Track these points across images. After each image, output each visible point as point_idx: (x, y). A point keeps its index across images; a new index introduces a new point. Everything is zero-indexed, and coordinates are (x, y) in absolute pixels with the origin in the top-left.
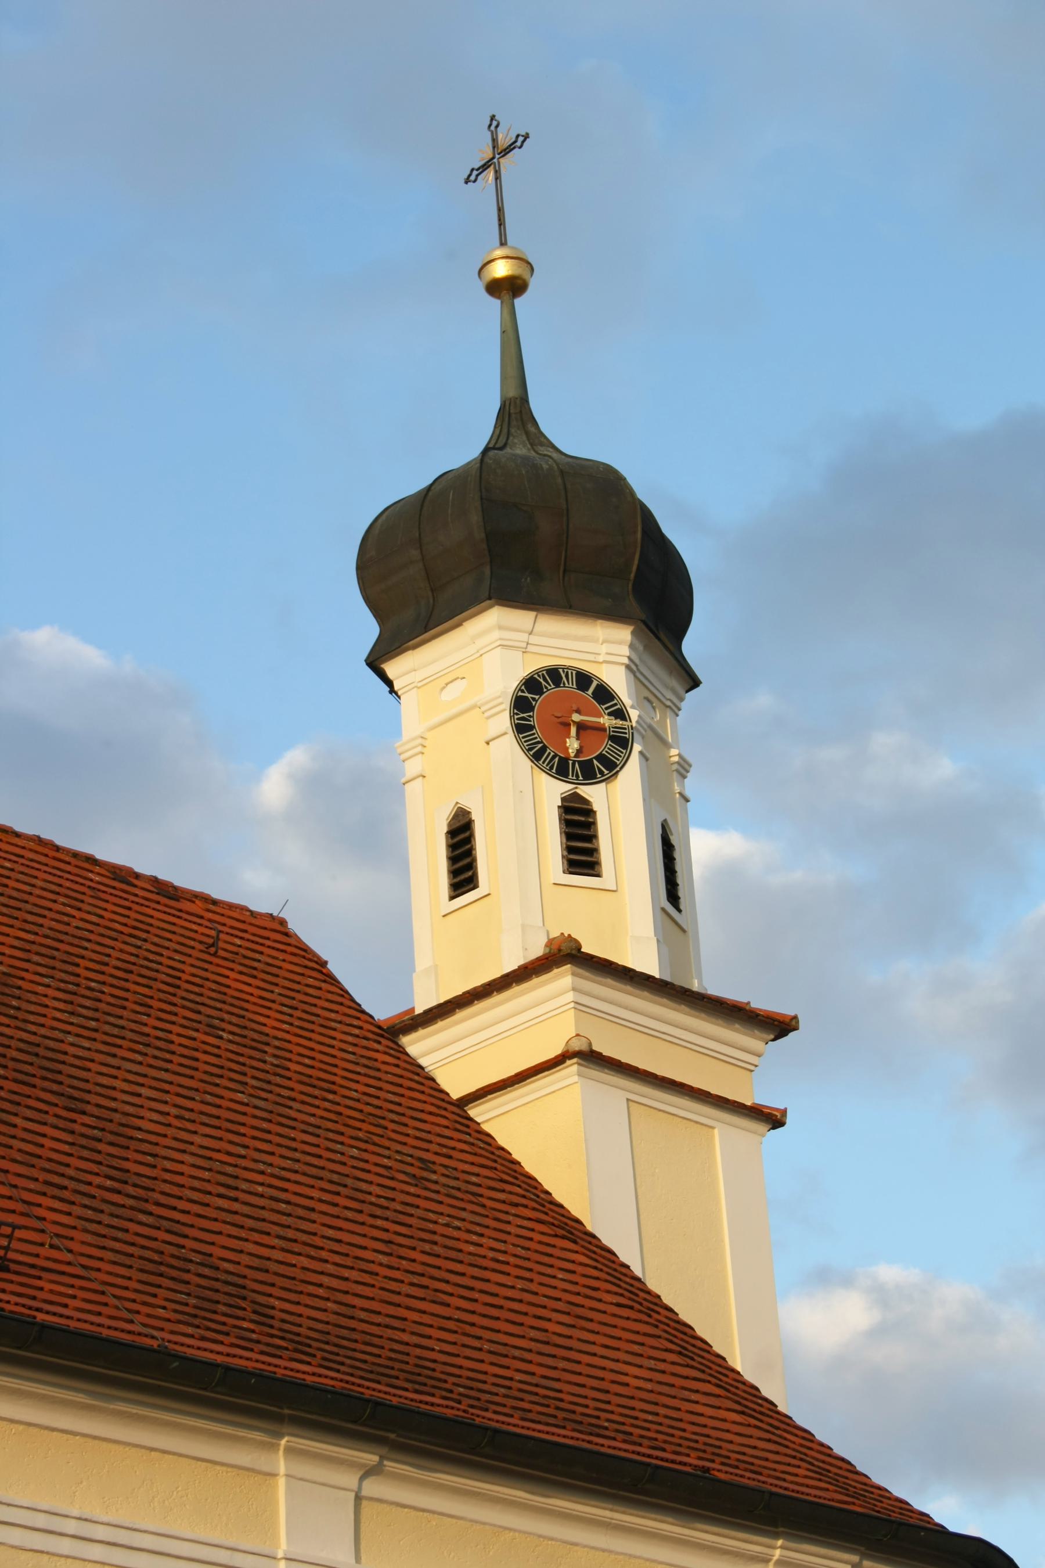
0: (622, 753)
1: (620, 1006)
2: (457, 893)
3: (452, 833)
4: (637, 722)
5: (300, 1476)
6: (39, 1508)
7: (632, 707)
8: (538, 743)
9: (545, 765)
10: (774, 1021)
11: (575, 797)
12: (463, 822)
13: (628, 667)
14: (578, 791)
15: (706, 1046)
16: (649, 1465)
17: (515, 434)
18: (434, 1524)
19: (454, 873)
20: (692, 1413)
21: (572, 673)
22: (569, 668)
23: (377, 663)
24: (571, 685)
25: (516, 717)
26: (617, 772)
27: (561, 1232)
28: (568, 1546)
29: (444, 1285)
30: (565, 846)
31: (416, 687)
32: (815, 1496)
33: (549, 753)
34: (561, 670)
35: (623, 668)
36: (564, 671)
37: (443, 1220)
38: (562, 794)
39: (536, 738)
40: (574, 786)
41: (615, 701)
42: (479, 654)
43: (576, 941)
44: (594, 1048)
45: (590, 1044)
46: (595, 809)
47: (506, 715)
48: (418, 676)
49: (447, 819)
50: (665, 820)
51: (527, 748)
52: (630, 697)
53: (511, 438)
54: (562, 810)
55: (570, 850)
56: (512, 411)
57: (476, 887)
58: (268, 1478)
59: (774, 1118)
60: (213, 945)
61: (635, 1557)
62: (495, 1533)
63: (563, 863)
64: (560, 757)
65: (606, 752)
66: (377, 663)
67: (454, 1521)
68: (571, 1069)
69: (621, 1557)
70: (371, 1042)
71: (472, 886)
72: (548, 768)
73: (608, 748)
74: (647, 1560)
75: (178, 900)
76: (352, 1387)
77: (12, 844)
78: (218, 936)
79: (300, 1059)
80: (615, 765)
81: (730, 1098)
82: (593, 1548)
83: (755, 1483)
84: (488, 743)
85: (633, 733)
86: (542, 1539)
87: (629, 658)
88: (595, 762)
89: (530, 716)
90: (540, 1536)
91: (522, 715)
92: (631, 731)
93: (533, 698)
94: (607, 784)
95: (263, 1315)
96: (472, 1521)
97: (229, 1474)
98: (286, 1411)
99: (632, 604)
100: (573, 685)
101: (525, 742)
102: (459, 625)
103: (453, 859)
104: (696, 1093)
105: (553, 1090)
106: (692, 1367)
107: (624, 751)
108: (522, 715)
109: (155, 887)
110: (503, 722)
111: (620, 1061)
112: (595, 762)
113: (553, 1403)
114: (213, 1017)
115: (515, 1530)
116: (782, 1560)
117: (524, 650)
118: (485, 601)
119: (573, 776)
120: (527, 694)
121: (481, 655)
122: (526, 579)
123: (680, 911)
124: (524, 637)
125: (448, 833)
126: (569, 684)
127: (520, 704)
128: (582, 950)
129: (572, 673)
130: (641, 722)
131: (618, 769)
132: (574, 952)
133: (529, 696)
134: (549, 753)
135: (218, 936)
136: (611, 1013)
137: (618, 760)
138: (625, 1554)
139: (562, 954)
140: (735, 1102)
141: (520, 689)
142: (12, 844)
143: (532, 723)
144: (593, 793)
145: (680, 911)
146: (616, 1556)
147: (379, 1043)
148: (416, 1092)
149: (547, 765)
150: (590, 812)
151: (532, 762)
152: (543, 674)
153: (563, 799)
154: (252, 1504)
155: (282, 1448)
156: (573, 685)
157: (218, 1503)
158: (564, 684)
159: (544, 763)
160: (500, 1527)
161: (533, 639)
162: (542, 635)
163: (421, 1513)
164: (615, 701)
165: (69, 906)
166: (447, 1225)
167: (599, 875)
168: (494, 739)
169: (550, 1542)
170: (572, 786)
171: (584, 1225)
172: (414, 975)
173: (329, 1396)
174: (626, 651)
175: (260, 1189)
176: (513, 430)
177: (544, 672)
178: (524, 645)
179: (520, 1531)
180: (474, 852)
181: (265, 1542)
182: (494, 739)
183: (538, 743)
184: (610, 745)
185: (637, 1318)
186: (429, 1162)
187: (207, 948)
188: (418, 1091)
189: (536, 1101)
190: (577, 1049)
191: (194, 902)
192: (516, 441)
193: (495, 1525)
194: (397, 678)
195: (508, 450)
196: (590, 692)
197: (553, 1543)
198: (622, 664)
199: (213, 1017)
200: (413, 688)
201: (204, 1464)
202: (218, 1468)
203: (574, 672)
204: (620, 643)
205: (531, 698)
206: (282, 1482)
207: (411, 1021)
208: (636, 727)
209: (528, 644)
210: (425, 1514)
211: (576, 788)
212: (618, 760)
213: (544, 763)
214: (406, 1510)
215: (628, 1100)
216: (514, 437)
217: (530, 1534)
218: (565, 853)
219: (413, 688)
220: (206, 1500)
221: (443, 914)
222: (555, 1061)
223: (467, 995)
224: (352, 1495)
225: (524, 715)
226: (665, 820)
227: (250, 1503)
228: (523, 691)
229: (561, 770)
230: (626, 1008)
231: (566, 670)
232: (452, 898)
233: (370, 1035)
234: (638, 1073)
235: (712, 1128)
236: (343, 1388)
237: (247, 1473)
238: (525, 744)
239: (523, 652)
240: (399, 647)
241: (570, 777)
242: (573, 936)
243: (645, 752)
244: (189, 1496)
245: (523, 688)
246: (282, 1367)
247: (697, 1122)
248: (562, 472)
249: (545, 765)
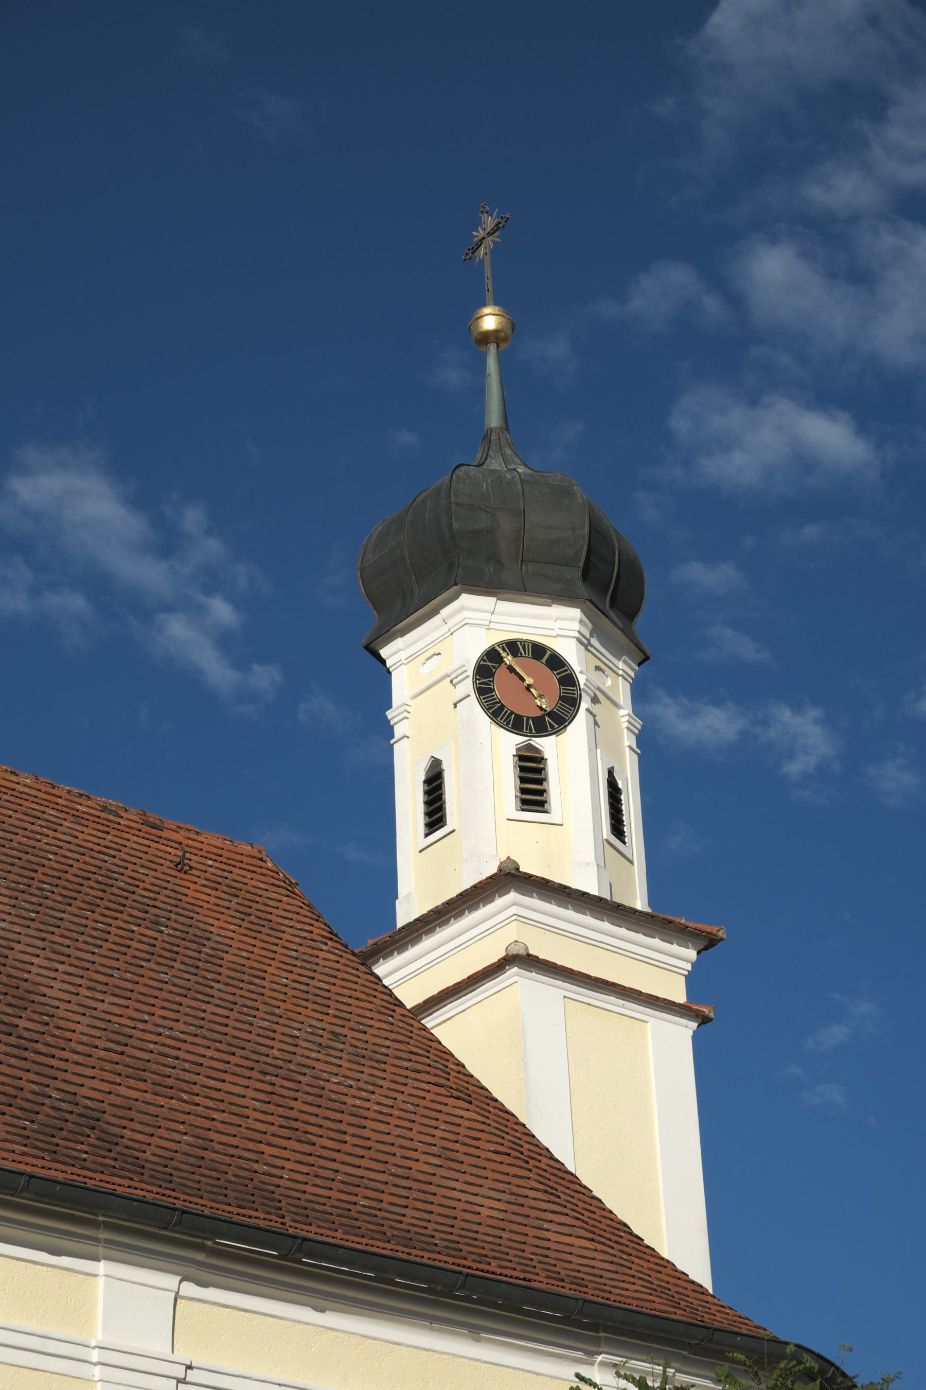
0: (571, 710)
1: (559, 919)
2: (432, 830)
3: (427, 782)
4: (585, 684)
5: (119, 1277)
6: (54, 1336)
7: (581, 672)
8: (497, 703)
9: (502, 721)
10: (703, 932)
11: (530, 747)
12: (436, 770)
13: (578, 640)
14: (531, 742)
15: (632, 950)
16: (460, 1273)
17: (493, 456)
18: (256, 1322)
19: (428, 814)
20: (539, 1238)
21: (528, 645)
22: (526, 641)
23: (372, 645)
24: (527, 655)
25: (478, 682)
26: (566, 726)
27: (456, 1093)
28: (392, 1345)
29: (316, 1128)
30: (518, 788)
31: (403, 664)
32: (482, 1271)
33: (507, 711)
34: (519, 643)
35: (574, 640)
36: (521, 644)
37: (336, 1079)
38: (516, 745)
39: (495, 699)
40: (528, 738)
41: (566, 668)
42: (450, 633)
43: (518, 865)
44: (531, 952)
45: (527, 949)
46: (545, 757)
47: (470, 681)
48: (403, 655)
49: (424, 771)
50: (612, 768)
51: (487, 707)
52: (579, 664)
53: (489, 459)
54: (517, 758)
55: (523, 791)
56: (492, 439)
57: (445, 824)
58: (88, 1277)
59: (701, 1014)
60: (179, 863)
61: (460, 1356)
62: (317, 1332)
63: (516, 802)
64: (516, 714)
65: (557, 709)
66: (372, 645)
67: (276, 1320)
68: (513, 972)
69: (445, 1356)
70: (318, 943)
71: (441, 824)
72: (505, 723)
73: (559, 707)
74: (472, 1359)
75: (162, 830)
76: (488, 1275)
77: (8, 780)
78: (184, 855)
79: (238, 952)
80: (564, 721)
81: (660, 996)
82: (416, 1347)
83: (555, 1288)
84: (455, 706)
85: (581, 694)
86: (365, 1339)
87: (579, 632)
88: (547, 718)
89: (490, 681)
90: (363, 1336)
91: (483, 680)
92: (579, 692)
93: (486, 661)
94: (557, 736)
95: (109, 1142)
96: (294, 1321)
97: (48, 1273)
98: (101, 1218)
99: (581, 587)
100: (529, 655)
101: (485, 702)
102: (435, 612)
103: (427, 803)
104: (628, 992)
105: (499, 989)
106: (558, 1204)
107: (573, 709)
108: (483, 680)
109: (141, 819)
110: (468, 687)
111: (556, 964)
112: (547, 718)
113: (335, 1211)
114: (159, 916)
115: (338, 1330)
116: (605, 1362)
117: (487, 627)
118: (453, 586)
119: (526, 730)
120: (488, 663)
121: (452, 634)
122: (490, 569)
123: (624, 843)
124: (487, 616)
125: (425, 782)
126: (525, 654)
127: (483, 691)
128: (520, 870)
129: (528, 645)
130: (588, 683)
131: (567, 724)
132: (513, 872)
133: (490, 664)
134: (507, 711)
135: (184, 855)
136: (664, 961)
137: (567, 716)
138: (449, 1354)
139: (502, 873)
140: (665, 999)
141: (482, 659)
142: (8, 780)
143: (492, 687)
144: (546, 744)
145: (624, 843)
146: (440, 1355)
147: (326, 944)
148: (349, 983)
149: (504, 722)
150: (542, 760)
151: (491, 719)
152: (503, 646)
153: (517, 750)
154: (71, 1300)
155: (597, 1363)
156: (529, 655)
157: (35, 1298)
158: (521, 654)
159: (501, 719)
160: (322, 1327)
161: (495, 618)
162: (503, 614)
163: (243, 1313)
164: (566, 668)
165: (46, 828)
166: (339, 1084)
167: (546, 812)
168: (460, 701)
169: (373, 1342)
170: (526, 738)
171: (487, 1090)
172: (397, 901)
173: (135, 1204)
174: (576, 626)
175: (151, 1046)
176: (491, 453)
177: (504, 645)
178: (487, 623)
179: (343, 1331)
180: (443, 796)
181: (82, 1333)
182: (460, 701)
183: (497, 703)
184: (560, 704)
185: (511, 1163)
186: (342, 1035)
187: (175, 866)
188: (352, 982)
189: (486, 1000)
190: (515, 953)
191: (178, 832)
192: (493, 461)
193: (317, 1325)
194: (387, 658)
195: (485, 467)
196: (544, 660)
197: (376, 1342)
198: (574, 637)
199: (159, 916)
200: (401, 665)
201: (23, 1263)
202: (38, 1267)
203: (530, 645)
204: (572, 619)
205: (486, 662)
206: (101, 1281)
207: (389, 938)
208: (583, 689)
209: (490, 622)
210: (247, 1314)
211: (530, 740)
212: (567, 716)
213: (501, 719)
214: (228, 1310)
215: (564, 997)
216: (492, 458)
217: (353, 1333)
218: (519, 794)
219: (401, 665)
220: (24, 1294)
221: (420, 849)
222: (498, 964)
223: (432, 913)
224: (173, 1294)
225: (486, 680)
226: (612, 768)
227: (69, 1298)
228: (484, 661)
229: (516, 724)
230: (565, 920)
231: (523, 643)
232: (427, 835)
233: (320, 938)
234: (573, 974)
235: (646, 1022)
236: (154, 1198)
237: (68, 1273)
238: (485, 704)
239: (487, 629)
240: (389, 630)
241: (525, 731)
242: (512, 858)
243: (590, 708)
244: (7, 1291)
245: (485, 658)
246: (474, 1268)
247: (631, 1017)
248: (522, 481)
249: (502, 721)
